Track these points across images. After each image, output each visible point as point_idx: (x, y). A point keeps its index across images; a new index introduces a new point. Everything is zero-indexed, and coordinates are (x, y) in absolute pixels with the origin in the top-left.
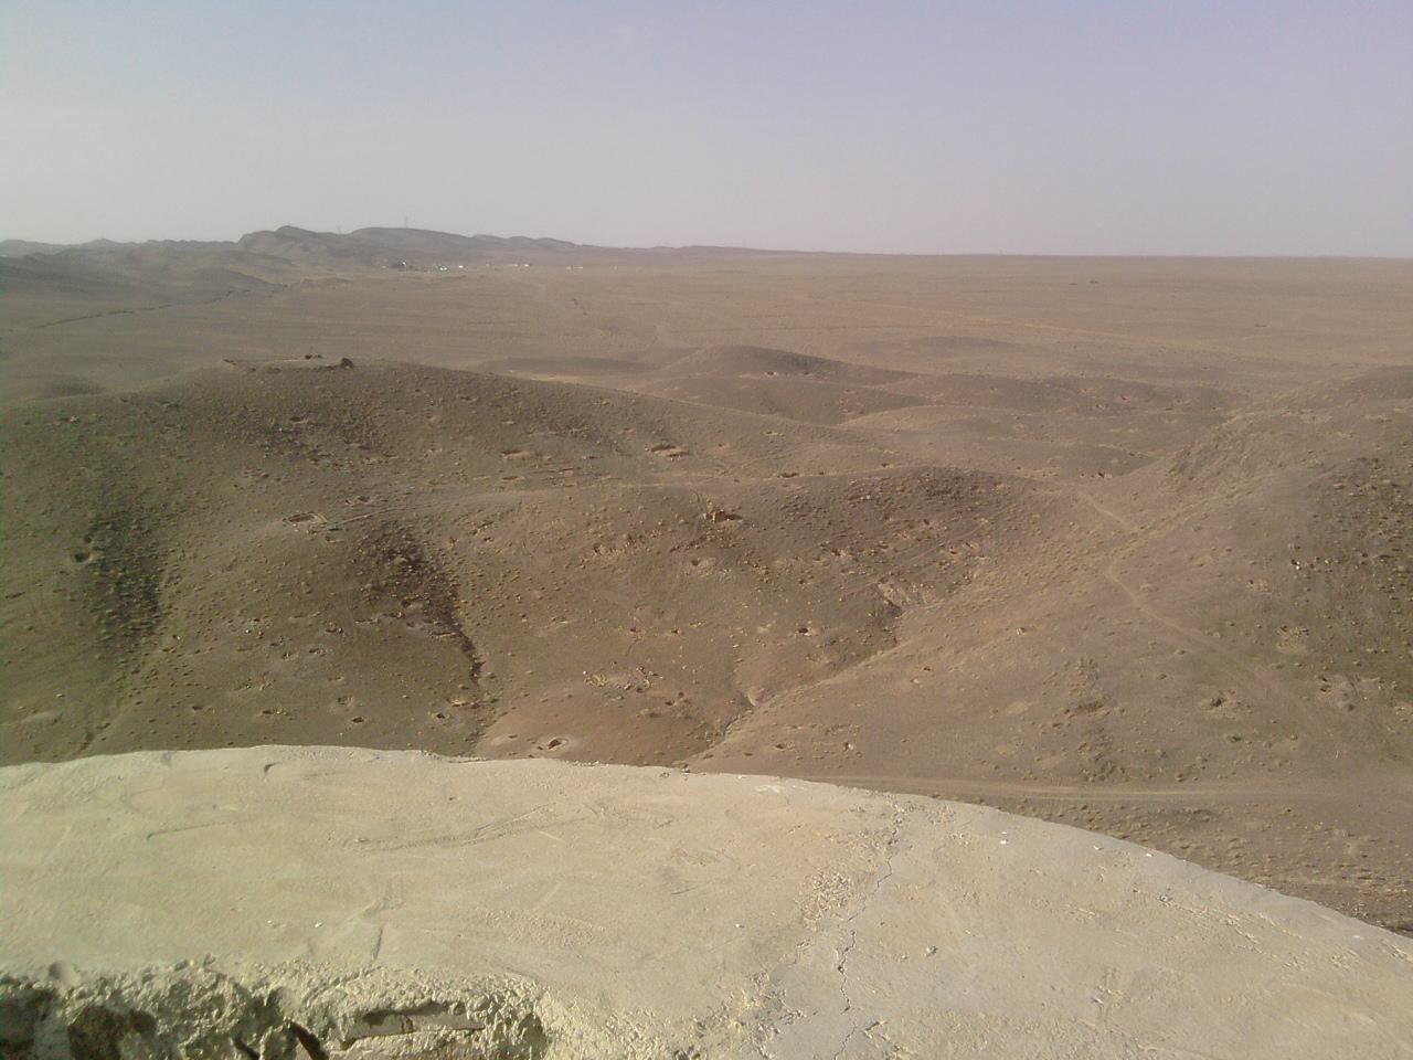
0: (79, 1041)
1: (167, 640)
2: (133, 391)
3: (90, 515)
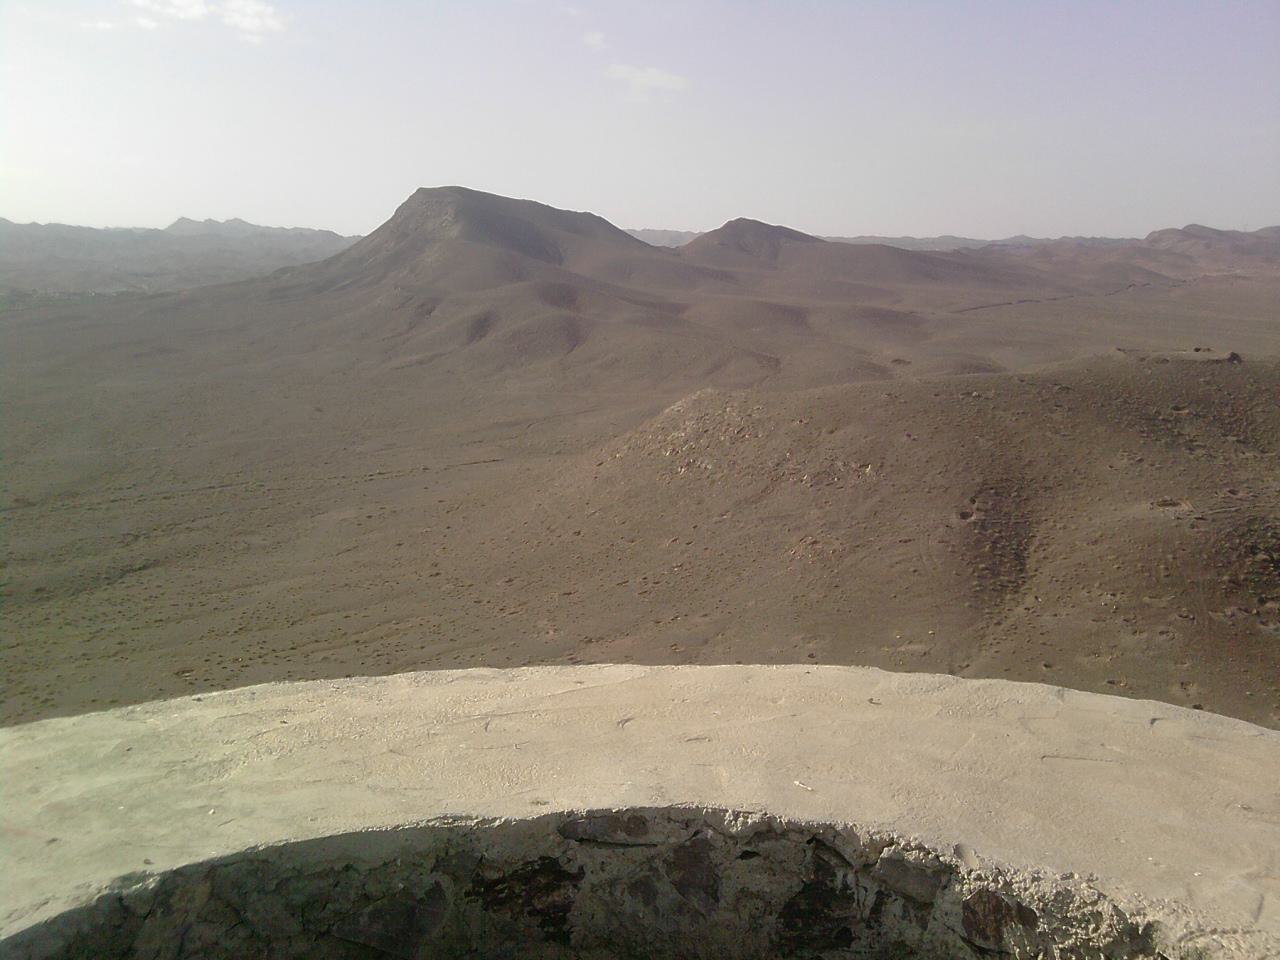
0: (970, 916)
1: (1029, 600)
2: (1030, 373)
3: (979, 480)
